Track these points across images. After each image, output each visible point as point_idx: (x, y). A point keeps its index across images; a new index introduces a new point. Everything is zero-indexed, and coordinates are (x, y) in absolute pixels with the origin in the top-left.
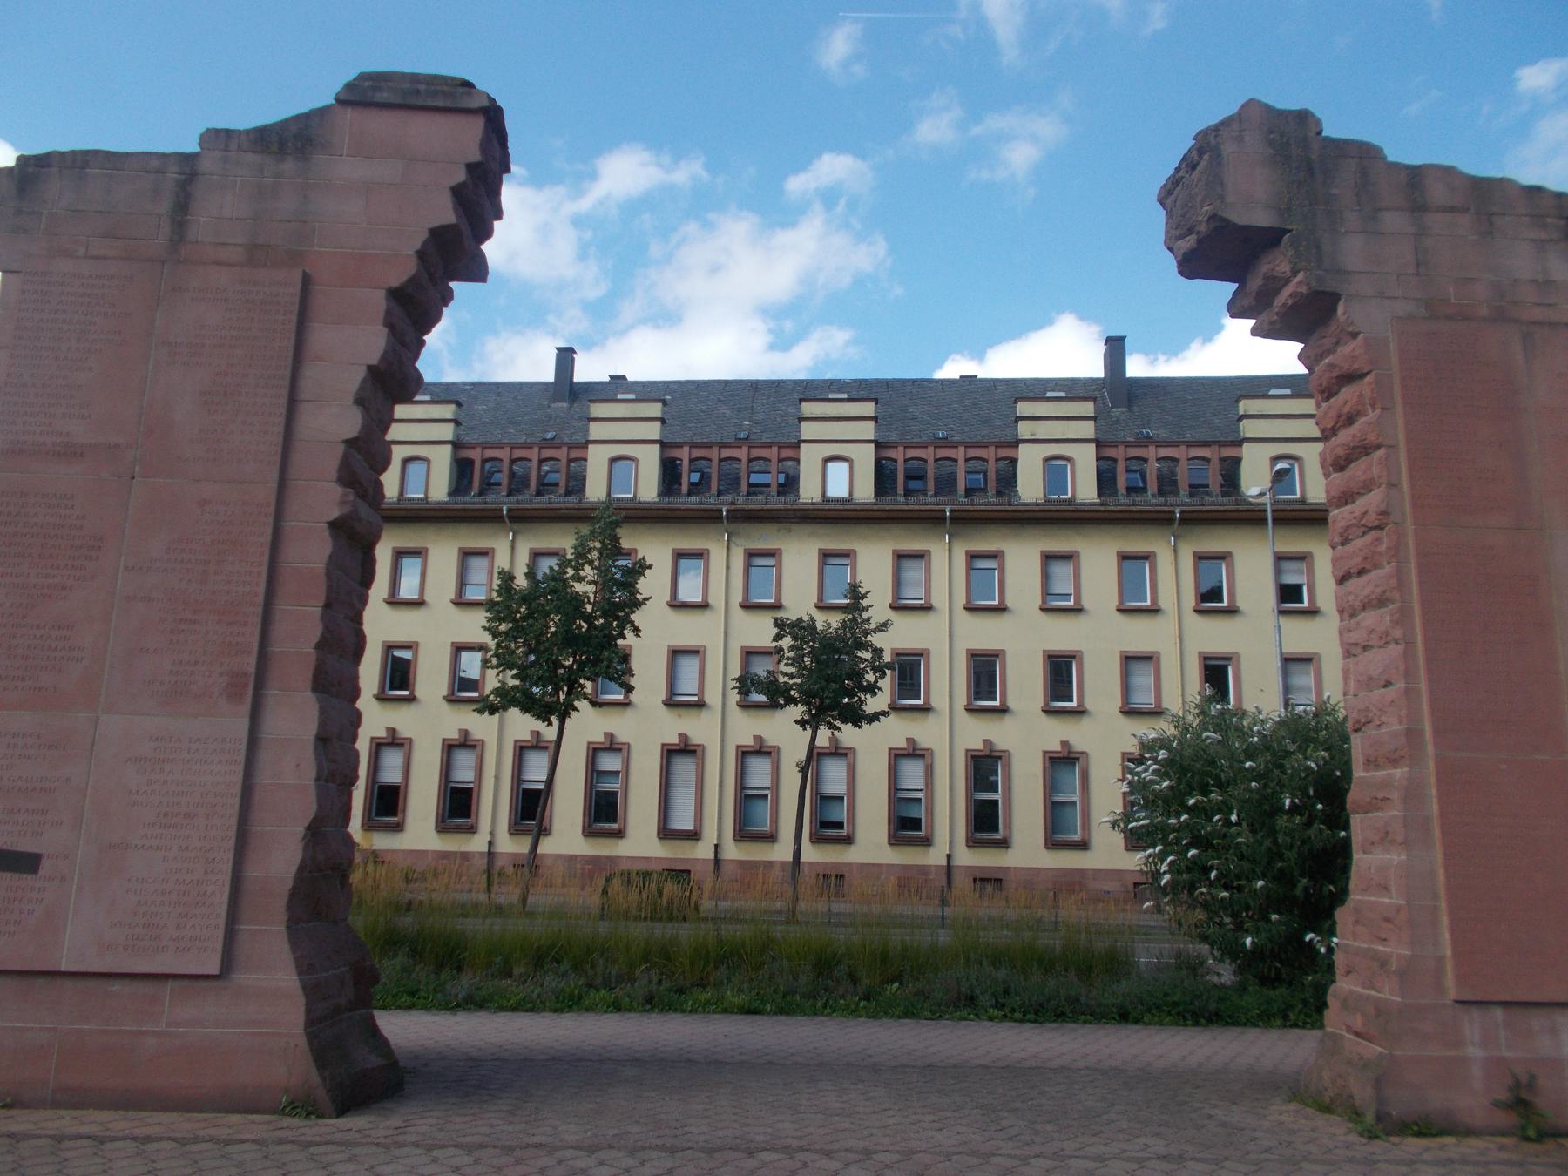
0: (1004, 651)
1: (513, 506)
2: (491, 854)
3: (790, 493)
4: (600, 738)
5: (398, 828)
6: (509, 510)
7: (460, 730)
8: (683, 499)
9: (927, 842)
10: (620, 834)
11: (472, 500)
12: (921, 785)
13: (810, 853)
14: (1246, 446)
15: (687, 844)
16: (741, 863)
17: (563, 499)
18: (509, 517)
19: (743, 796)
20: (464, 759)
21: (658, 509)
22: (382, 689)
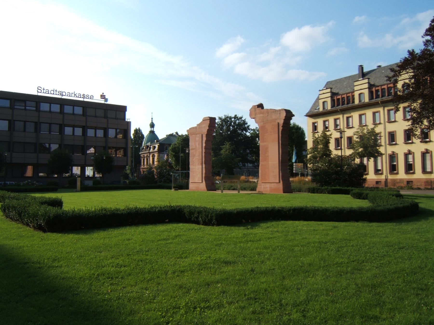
0: (396, 131)
1: (381, 101)
2: (386, 180)
3: (182, 142)
4: (406, 151)
5: (397, 173)
6: (380, 102)
7: (391, 151)
8: (375, 100)
9: (382, 174)
10: (397, 173)
11: (374, 101)
12: (412, 161)
13: (390, 177)
14: (355, 92)
15: (380, 176)
16: (391, 179)
17: (352, 104)
18: (340, 111)
19: (407, 164)
20: (410, 157)
21: (368, 104)
22: (336, 148)
